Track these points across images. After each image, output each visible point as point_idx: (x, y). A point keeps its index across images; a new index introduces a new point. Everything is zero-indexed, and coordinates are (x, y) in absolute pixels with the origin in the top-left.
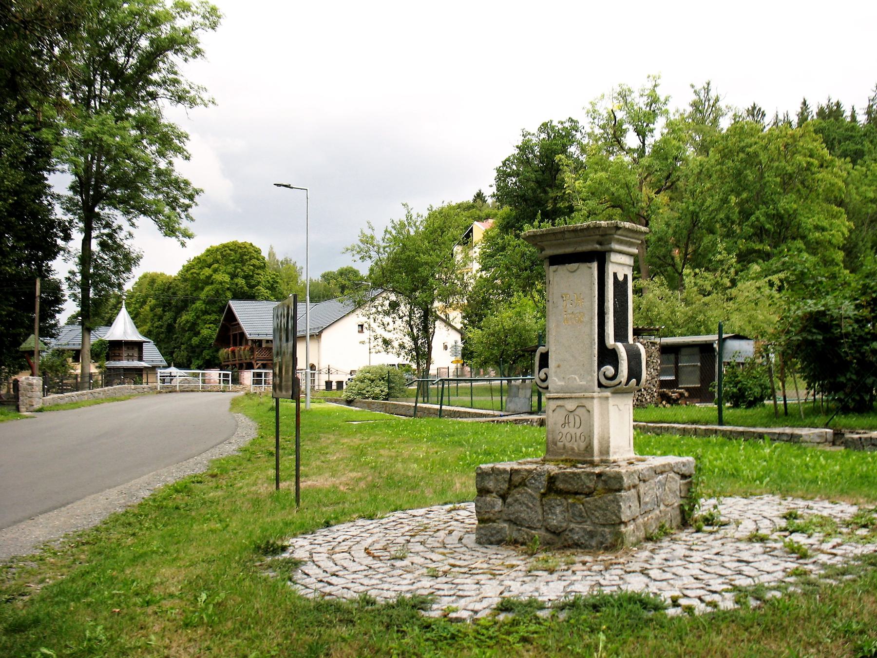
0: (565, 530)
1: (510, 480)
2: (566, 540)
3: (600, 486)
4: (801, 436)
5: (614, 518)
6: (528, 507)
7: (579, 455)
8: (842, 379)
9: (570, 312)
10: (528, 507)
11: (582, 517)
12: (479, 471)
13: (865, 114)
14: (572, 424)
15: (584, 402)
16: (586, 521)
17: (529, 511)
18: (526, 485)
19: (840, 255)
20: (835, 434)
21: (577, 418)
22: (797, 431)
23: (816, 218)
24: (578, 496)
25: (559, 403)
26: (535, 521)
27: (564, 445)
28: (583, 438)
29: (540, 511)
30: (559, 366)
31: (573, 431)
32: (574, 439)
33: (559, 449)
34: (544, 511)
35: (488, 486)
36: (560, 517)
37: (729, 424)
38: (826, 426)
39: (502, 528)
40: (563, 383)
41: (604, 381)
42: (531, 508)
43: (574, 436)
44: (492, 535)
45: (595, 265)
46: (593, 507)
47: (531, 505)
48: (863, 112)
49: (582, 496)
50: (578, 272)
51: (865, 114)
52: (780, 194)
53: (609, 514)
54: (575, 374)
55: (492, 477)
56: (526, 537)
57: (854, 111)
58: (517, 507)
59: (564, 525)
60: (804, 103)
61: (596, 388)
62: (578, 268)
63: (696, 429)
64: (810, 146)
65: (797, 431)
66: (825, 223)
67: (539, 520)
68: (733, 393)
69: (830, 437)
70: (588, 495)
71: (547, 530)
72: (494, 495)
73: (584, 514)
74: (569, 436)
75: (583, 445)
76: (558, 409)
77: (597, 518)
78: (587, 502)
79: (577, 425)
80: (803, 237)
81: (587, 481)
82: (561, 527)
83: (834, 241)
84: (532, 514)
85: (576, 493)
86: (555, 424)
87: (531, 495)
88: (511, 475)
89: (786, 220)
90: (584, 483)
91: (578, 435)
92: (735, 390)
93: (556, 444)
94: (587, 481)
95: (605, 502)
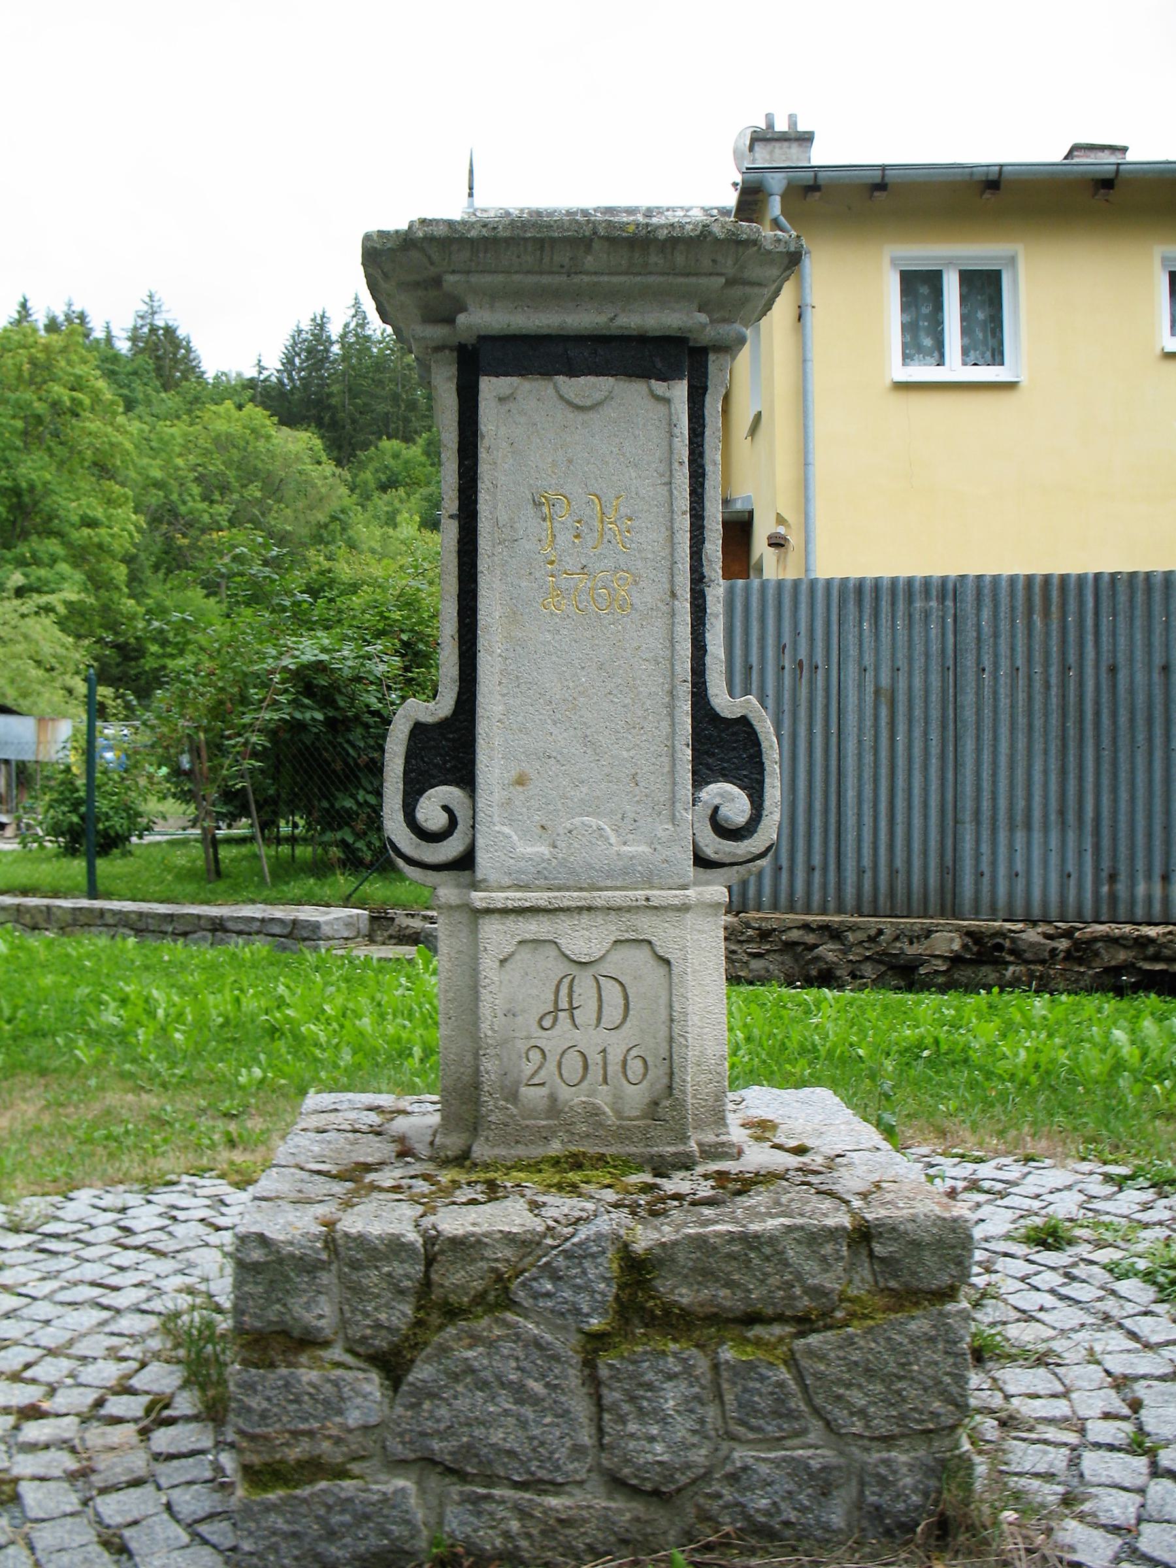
0: (706, 1476)
1: (427, 1284)
2: (705, 1517)
3: (861, 1283)
4: (316, 926)
5: (936, 1405)
6: (520, 1394)
7: (622, 1134)
8: (349, 803)
9: (570, 563)
10: (520, 1394)
11: (791, 1415)
12: (257, 1255)
13: (129, 339)
14: (586, 1015)
15: (646, 925)
16: (804, 1432)
17: (528, 1412)
18: (510, 1304)
19: (120, 572)
20: (373, 919)
21: (612, 992)
22: (307, 913)
23: (84, 501)
24: (758, 1331)
25: (533, 928)
26: (561, 1454)
27: (553, 1098)
28: (635, 1067)
29: (581, 1407)
30: (521, 781)
31: (590, 1040)
32: (596, 1072)
33: (531, 1114)
34: (600, 1407)
35: (309, 1317)
36: (682, 1428)
37: (108, 896)
38: (347, 902)
39: (385, 1499)
40: (544, 850)
41: (713, 846)
42: (535, 1400)
43: (595, 1058)
44: (332, 1535)
45: (680, 391)
46: (834, 1371)
47: (536, 1387)
48: (125, 335)
49: (778, 1330)
50: (609, 411)
51: (129, 339)
52: (17, 449)
53: (912, 1392)
54: (597, 814)
55: (325, 1278)
56: (515, 1525)
57: (109, 332)
58: (467, 1401)
59: (700, 1456)
60: (24, 305)
61: (690, 870)
62: (609, 397)
63: (48, 907)
64: (78, 371)
65: (307, 913)
66: (99, 513)
67: (578, 1451)
68: (71, 824)
69: (364, 926)
70: (805, 1324)
71: (616, 1483)
72: (336, 1353)
73: (797, 1403)
74: (573, 1062)
75: (636, 1096)
76: (525, 954)
77: (862, 1413)
78: (810, 1353)
79: (613, 1013)
80: (60, 534)
81: (811, 1267)
82: (688, 1466)
83: (116, 546)
84: (547, 1428)
85: (752, 1319)
86: (510, 1013)
87: (537, 1344)
88: (430, 1261)
89: (27, 499)
90: (799, 1277)
91: (615, 1057)
92: (75, 819)
93: (513, 1096)
94: (811, 1267)
95: (893, 1348)
